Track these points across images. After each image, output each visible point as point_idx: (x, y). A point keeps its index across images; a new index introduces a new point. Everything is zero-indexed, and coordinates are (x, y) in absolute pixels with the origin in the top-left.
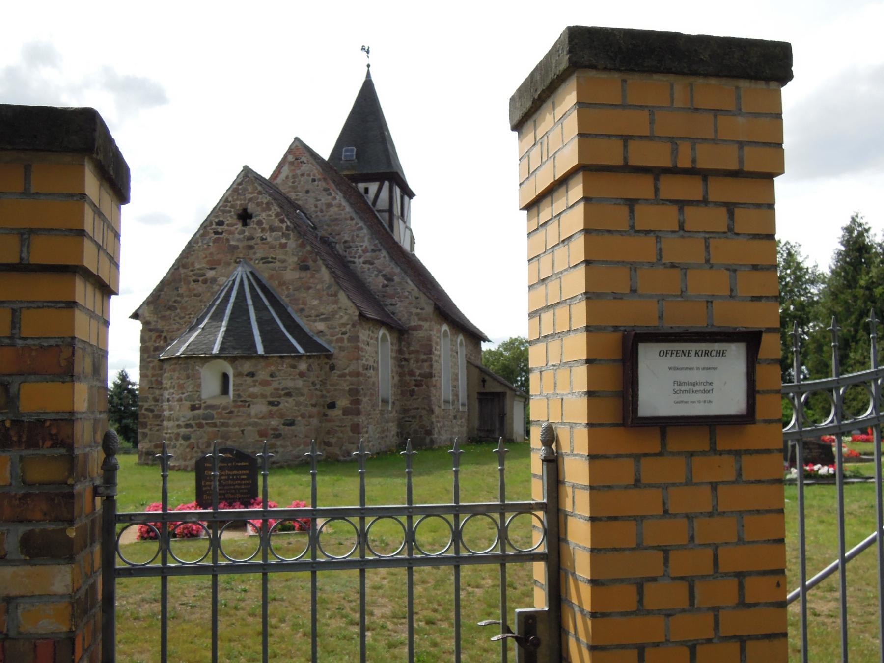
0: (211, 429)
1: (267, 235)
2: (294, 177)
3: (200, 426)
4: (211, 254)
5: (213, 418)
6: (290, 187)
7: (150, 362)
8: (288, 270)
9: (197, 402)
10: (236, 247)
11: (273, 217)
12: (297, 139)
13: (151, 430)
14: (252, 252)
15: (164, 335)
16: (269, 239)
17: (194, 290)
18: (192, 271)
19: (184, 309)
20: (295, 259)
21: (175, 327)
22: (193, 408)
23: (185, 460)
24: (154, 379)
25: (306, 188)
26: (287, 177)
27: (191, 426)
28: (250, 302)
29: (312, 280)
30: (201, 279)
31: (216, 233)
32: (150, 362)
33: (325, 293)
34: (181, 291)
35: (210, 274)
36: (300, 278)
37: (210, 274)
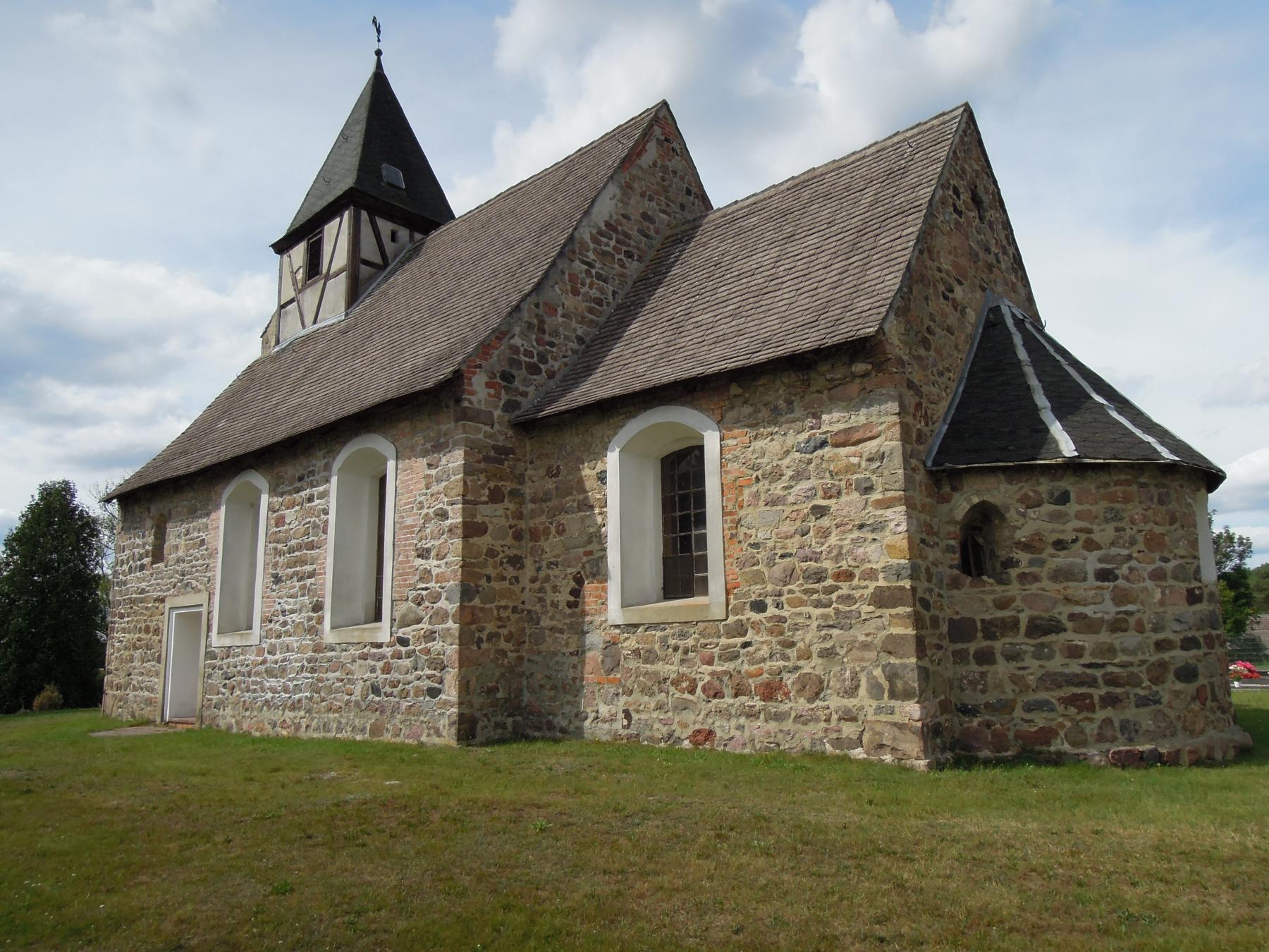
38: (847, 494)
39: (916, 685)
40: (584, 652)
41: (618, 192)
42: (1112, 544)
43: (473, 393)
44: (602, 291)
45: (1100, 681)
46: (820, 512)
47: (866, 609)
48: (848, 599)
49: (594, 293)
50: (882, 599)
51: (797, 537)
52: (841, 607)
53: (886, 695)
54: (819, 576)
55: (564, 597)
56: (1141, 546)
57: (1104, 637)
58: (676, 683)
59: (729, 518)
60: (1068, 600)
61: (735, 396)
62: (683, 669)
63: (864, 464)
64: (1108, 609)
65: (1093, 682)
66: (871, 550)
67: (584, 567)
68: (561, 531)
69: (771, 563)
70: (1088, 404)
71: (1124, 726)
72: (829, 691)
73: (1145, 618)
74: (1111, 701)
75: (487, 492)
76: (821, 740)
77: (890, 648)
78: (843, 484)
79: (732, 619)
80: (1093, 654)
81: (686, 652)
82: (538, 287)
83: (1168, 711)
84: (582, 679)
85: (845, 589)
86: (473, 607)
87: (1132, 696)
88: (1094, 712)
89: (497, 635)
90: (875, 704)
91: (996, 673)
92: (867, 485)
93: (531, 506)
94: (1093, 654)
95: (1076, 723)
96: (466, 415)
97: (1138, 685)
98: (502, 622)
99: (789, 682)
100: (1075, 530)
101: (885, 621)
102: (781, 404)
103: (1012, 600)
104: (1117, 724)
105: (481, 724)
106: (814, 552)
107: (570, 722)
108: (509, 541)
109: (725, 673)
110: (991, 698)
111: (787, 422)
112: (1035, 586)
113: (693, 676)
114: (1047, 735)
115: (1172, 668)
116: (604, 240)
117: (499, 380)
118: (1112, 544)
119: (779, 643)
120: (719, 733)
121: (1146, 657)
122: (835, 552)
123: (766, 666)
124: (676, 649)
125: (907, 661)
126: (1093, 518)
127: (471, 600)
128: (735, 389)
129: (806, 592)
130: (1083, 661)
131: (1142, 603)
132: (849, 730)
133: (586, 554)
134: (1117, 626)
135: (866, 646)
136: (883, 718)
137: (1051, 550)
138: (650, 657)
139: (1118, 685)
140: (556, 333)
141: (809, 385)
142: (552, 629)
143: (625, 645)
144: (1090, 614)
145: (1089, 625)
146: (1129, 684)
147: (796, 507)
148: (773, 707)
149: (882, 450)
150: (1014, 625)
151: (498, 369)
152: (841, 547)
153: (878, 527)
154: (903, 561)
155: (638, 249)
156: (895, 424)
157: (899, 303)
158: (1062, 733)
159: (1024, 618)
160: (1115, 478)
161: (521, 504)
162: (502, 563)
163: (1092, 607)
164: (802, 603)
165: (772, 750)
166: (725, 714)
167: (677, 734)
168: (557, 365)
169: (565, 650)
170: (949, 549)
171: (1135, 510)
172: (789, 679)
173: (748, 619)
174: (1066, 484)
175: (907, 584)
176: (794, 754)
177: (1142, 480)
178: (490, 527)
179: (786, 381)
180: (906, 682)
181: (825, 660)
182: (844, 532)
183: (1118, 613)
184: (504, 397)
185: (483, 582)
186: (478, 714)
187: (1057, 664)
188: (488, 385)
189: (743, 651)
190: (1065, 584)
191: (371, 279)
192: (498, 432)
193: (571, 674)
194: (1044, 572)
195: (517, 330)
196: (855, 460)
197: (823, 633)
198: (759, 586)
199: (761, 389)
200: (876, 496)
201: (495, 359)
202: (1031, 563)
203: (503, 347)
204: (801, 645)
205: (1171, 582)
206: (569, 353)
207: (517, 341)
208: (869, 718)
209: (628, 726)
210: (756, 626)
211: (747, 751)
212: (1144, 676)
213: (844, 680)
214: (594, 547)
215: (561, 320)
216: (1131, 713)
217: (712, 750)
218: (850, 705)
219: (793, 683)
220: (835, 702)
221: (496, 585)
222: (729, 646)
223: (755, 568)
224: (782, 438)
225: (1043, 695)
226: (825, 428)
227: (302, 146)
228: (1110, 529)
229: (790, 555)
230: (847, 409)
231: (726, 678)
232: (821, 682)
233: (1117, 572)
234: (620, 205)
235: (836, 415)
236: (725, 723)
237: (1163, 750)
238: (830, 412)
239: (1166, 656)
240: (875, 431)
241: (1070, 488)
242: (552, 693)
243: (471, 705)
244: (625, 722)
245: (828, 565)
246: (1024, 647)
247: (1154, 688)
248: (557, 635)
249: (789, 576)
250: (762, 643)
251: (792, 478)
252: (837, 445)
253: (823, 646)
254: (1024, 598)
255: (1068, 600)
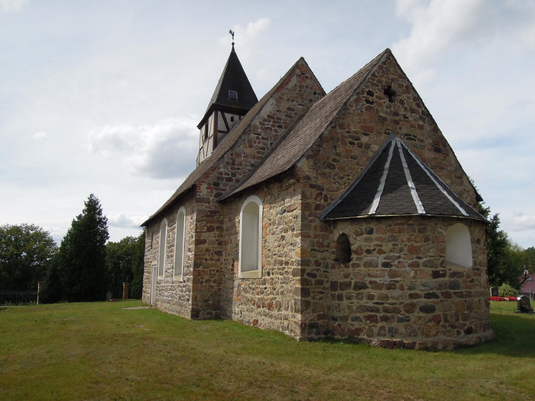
0: (457, 300)
1: (408, 114)
2: (301, 87)
3: (447, 296)
4: (364, 120)
5: (458, 287)
6: (297, 93)
7: (311, 221)
8: (426, 150)
9: (440, 268)
10: (385, 119)
11: (412, 100)
12: (302, 59)
13: (313, 298)
14: (398, 126)
15: (324, 193)
16: (410, 119)
17: (351, 151)
18: (348, 132)
19: (342, 169)
20: (431, 141)
21: (335, 186)
22: (436, 275)
23: (427, 336)
24: (315, 240)
25: (309, 98)
26: (295, 86)
27: (435, 296)
28: (405, 165)
29: (444, 162)
30: (356, 142)
31: (368, 101)
32: (311, 221)
33: (453, 174)
34: (338, 151)
35: (364, 139)
36: (435, 158)
37: (364, 139)
41: (274, 102)
42: (391, 251)
43: (200, 192)
44: (265, 144)
45: (381, 310)
49: (261, 145)
56: (406, 252)
57: (384, 291)
60: (369, 275)
64: (387, 279)
65: (378, 311)
70: (404, 187)
71: (391, 330)
73: (405, 284)
74: (385, 319)
75: (206, 228)
79: (263, 278)
80: (378, 299)
82: (232, 148)
83: (413, 325)
87: (396, 317)
88: (377, 323)
89: (210, 281)
91: (343, 304)
93: (225, 232)
94: (378, 299)
95: (370, 327)
96: (200, 200)
97: (399, 313)
98: (212, 276)
100: (374, 245)
103: (350, 274)
104: (387, 329)
108: (216, 245)
110: (341, 314)
112: (358, 268)
114: (358, 331)
115: (418, 306)
116: (266, 123)
117: (212, 186)
118: (391, 251)
121: (404, 301)
126: (382, 240)
127: (198, 268)
130: (374, 301)
131: (404, 277)
134: (390, 287)
137: (365, 254)
139: (389, 312)
140: (241, 164)
144: (378, 281)
145: (376, 286)
146: (395, 312)
150: (349, 285)
151: (212, 182)
155: (285, 123)
157: (310, 153)
158: (364, 331)
159: (353, 282)
160: (395, 222)
161: (222, 231)
162: (212, 254)
163: (379, 278)
168: (240, 177)
170: (333, 253)
171: (404, 236)
174: (372, 225)
175: (300, 267)
177: (410, 222)
178: (207, 241)
183: (391, 281)
184: (215, 192)
185: (204, 261)
186: (200, 309)
187: (364, 302)
188: (207, 188)
190: (369, 268)
191: (222, 138)
192: (213, 205)
194: (362, 263)
195: (222, 166)
201: (211, 178)
202: (357, 259)
203: (215, 173)
205: (422, 268)
206: (247, 171)
207: (222, 170)
212: (402, 309)
215: (243, 159)
216: (394, 325)
221: (209, 262)
225: (358, 315)
226: (286, 205)
227: (206, 87)
228: (390, 245)
233: (392, 263)
234: (276, 107)
237: (405, 342)
239: (415, 301)
241: (374, 227)
243: (197, 305)
246: (352, 294)
247: (407, 314)
254: (356, 272)
255: (369, 275)
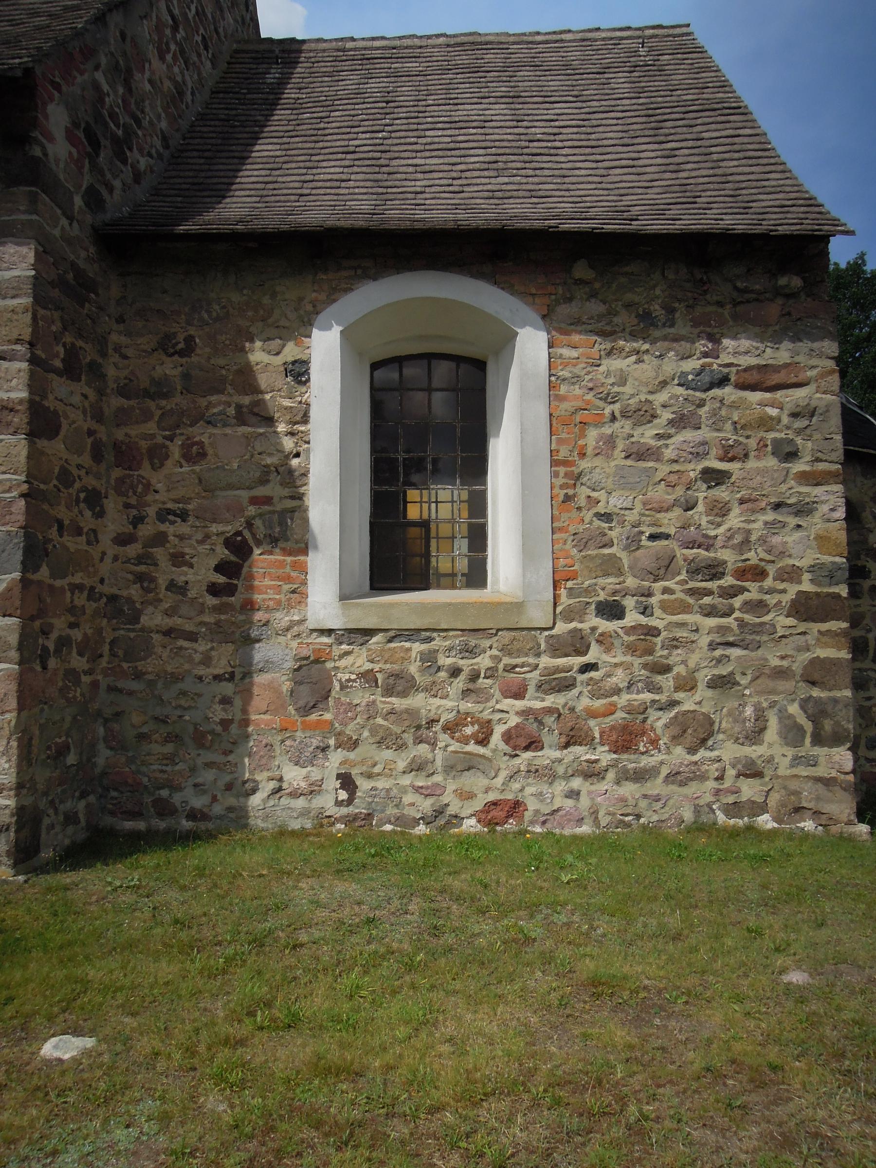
38: (758, 458)
39: (851, 726)
40: (247, 674)
46: (714, 478)
47: (783, 622)
48: (758, 607)
50: (806, 609)
51: (678, 511)
52: (748, 617)
53: (808, 740)
54: (714, 570)
55: (202, 573)
58: (451, 728)
59: (562, 470)
61: (580, 282)
62: (467, 706)
63: (785, 420)
66: (791, 539)
67: (249, 525)
68: (194, 454)
69: (633, 543)
72: (721, 736)
76: (709, 806)
77: (816, 676)
78: (752, 443)
81: (474, 677)
84: (246, 722)
85: (753, 592)
86: (40, 583)
90: (790, 752)
92: (788, 449)
93: (117, 402)
99: (659, 724)
101: (810, 639)
102: (657, 309)
105: (46, 821)
106: (706, 536)
107: (214, 799)
109: (549, 711)
111: (665, 338)
113: (486, 715)
119: (645, 666)
120: (532, 805)
122: (738, 539)
123: (623, 699)
124: (455, 672)
125: (838, 694)
128: (581, 270)
129: (692, 592)
132: (749, 790)
133: (254, 501)
135: (780, 673)
136: (803, 771)
138: (399, 684)
141: (706, 292)
142: (168, 633)
143: (342, 663)
147: (676, 467)
148: (629, 761)
149: (814, 403)
152: (749, 532)
153: (804, 510)
154: (838, 559)
156: (832, 372)
162: (78, 501)
164: (686, 609)
165: (628, 825)
166: (548, 774)
167: (451, 810)
169: (201, 671)
172: (659, 721)
173: (593, 629)
176: (672, 831)
179: (671, 276)
180: (837, 723)
181: (718, 691)
182: (753, 511)
186: (43, 804)
189: (581, 678)
193: (218, 713)
196: (773, 412)
197: (718, 653)
198: (611, 580)
199: (623, 280)
200: (800, 466)
204: (680, 669)
208: (781, 772)
209: (350, 801)
210: (605, 641)
211: (585, 829)
213: (744, 721)
214: (273, 489)
217: (523, 833)
218: (754, 756)
219: (666, 726)
220: (729, 751)
222: (558, 670)
223: (606, 551)
224: (656, 362)
229: (667, 537)
230: (761, 337)
231: (550, 720)
232: (712, 723)
235: (745, 343)
236: (545, 788)
238: (734, 337)
240: (801, 377)
242: (169, 748)
244: (343, 795)
245: (727, 555)
248: (181, 643)
249: (665, 567)
250: (616, 665)
251: (671, 422)
252: (743, 386)
253: (716, 672)
